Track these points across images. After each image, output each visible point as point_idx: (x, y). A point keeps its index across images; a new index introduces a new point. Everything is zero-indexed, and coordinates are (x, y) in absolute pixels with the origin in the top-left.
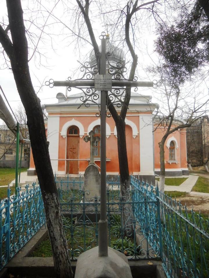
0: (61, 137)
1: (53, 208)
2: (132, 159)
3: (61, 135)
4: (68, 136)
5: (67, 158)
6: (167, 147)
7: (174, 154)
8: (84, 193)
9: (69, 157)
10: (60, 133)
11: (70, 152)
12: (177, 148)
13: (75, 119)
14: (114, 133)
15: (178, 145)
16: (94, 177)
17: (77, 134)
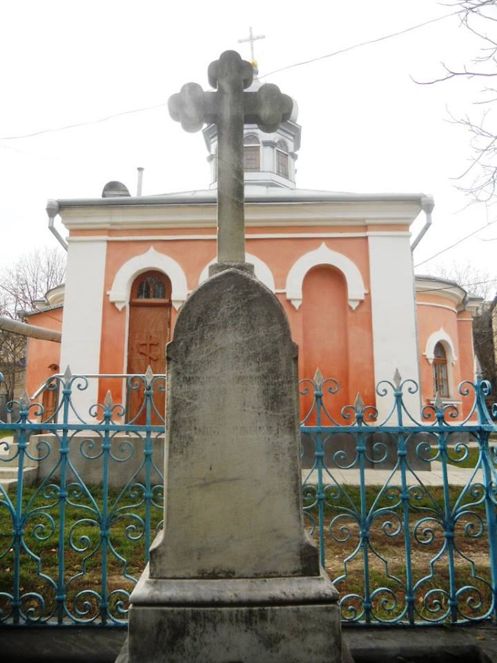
0: (109, 306)
1: (453, 364)
2: (347, 380)
3: (112, 299)
4: (132, 305)
5: (130, 370)
6: (427, 359)
7: (447, 380)
8: (399, 392)
9: (135, 367)
10: (108, 293)
11: (141, 357)
12: (454, 363)
13: (156, 249)
14: (285, 294)
15: (456, 355)
16: (251, 370)
17: (164, 297)
